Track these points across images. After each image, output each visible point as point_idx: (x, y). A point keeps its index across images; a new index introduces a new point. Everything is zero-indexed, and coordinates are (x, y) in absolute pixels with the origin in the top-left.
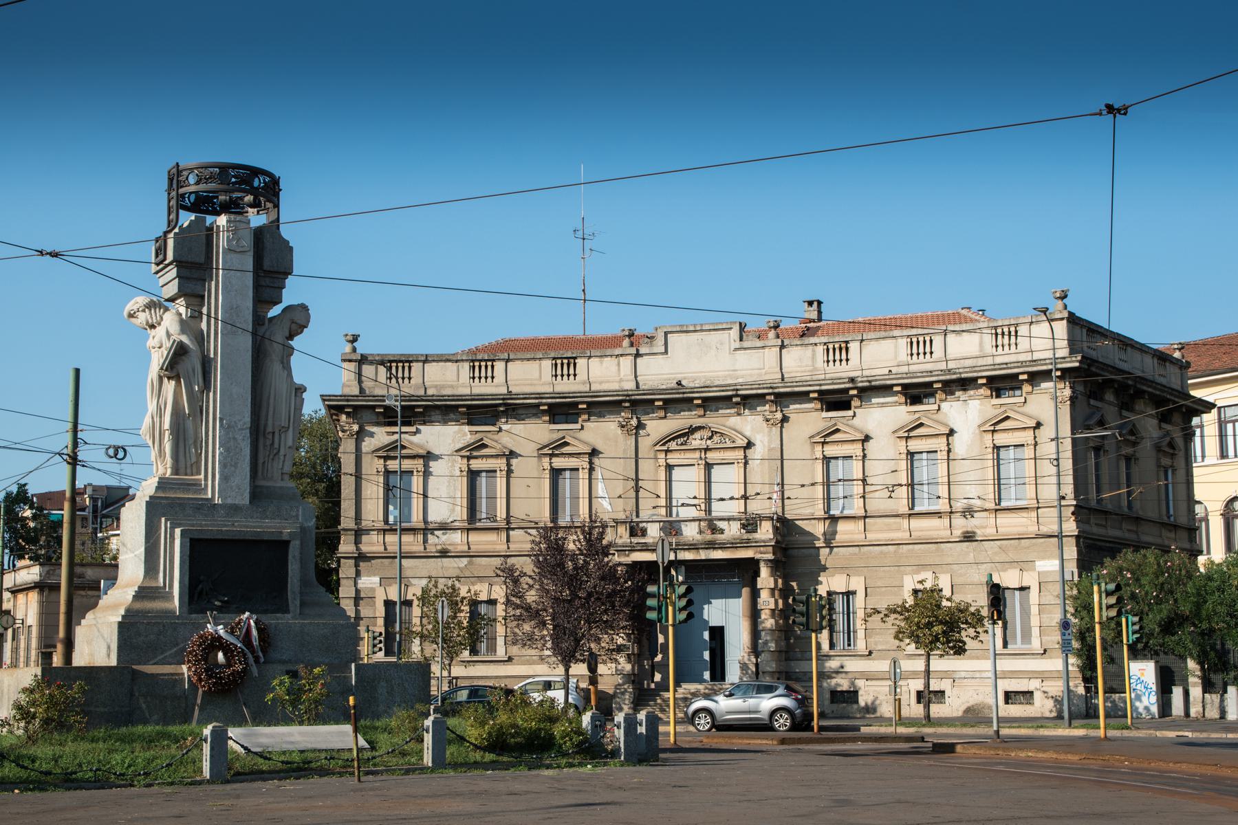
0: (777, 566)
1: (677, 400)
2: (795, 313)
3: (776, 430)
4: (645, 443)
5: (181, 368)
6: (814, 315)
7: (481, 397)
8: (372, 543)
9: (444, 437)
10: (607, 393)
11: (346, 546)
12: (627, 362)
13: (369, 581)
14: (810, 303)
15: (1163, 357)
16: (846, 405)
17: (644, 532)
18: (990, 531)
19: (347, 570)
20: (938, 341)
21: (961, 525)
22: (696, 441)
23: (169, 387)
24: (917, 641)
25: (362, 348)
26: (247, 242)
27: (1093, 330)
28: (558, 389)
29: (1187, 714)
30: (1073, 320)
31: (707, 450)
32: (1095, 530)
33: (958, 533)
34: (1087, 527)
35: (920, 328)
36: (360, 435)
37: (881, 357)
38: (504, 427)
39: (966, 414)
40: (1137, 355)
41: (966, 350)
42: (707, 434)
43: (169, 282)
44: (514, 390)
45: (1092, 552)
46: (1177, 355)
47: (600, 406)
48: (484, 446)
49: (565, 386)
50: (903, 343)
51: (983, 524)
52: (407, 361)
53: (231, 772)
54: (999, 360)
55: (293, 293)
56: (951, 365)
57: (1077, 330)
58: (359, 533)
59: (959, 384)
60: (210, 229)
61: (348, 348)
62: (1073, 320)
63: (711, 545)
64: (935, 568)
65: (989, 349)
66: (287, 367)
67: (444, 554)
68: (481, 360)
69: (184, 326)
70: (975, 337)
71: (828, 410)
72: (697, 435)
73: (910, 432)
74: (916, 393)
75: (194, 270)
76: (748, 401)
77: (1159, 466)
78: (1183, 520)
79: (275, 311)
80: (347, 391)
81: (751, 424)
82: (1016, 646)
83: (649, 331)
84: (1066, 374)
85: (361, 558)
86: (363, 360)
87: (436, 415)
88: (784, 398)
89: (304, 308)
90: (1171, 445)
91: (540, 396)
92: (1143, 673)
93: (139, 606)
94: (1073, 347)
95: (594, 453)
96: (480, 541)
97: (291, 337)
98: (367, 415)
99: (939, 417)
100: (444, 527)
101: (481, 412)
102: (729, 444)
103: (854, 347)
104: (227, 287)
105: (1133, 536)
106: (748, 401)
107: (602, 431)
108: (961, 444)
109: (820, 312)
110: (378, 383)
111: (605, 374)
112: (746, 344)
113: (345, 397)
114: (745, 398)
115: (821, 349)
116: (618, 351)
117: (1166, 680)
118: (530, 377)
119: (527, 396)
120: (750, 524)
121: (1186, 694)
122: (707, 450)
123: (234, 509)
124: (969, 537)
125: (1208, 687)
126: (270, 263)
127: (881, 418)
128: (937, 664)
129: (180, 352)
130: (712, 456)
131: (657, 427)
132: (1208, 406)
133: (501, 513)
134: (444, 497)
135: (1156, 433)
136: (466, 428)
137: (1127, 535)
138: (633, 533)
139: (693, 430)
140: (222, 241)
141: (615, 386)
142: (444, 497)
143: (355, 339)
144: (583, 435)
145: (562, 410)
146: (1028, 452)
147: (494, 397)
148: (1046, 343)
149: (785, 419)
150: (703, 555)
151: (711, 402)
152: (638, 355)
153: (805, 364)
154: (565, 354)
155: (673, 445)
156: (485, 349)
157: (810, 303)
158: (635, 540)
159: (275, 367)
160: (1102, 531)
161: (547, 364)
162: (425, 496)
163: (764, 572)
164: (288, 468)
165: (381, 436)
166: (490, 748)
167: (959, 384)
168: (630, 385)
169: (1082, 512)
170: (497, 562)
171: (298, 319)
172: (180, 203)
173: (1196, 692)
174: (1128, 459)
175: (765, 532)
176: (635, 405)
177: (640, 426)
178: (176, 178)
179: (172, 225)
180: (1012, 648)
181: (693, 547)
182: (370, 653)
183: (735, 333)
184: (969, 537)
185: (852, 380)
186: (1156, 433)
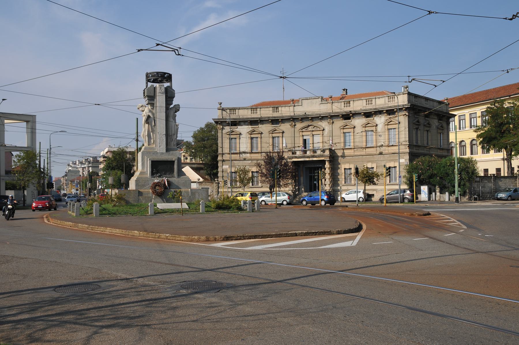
0: (330, 161)
1: (304, 118)
2: (339, 93)
3: (331, 125)
4: (296, 130)
5: (149, 121)
6: (345, 93)
7: (253, 118)
8: (226, 157)
9: (244, 129)
10: (286, 116)
11: (220, 158)
12: (292, 108)
13: (226, 167)
14: (344, 90)
15: (440, 103)
16: (349, 119)
17: (295, 153)
18: (387, 152)
19: (220, 164)
20: (374, 100)
21: (379, 150)
22: (310, 129)
23: (147, 125)
24: (362, 181)
25: (223, 106)
26: (163, 90)
27: (416, 96)
28: (274, 116)
29: (435, 200)
30: (409, 94)
31: (313, 131)
32: (415, 151)
33: (378, 152)
34: (412, 150)
35: (369, 97)
36: (223, 129)
37: (358, 106)
38: (260, 126)
39: (380, 120)
40: (432, 102)
41: (381, 103)
42: (312, 127)
43: (145, 101)
44: (263, 116)
45: (412, 156)
46: (446, 101)
47: (284, 120)
48: (255, 131)
49: (276, 115)
50: (365, 101)
51: (384, 150)
52: (234, 109)
53: (158, 212)
54: (389, 105)
55: (175, 102)
56: (377, 107)
57: (411, 97)
58: (223, 154)
59: (379, 112)
60: (155, 88)
61: (219, 106)
62: (409, 94)
63: (313, 157)
64: (372, 162)
65: (343, 107)
66: (175, 120)
67: (245, 159)
68: (254, 108)
69: (150, 111)
70: (383, 99)
71: (345, 120)
72: (310, 127)
73: (366, 125)
74: (368, 115)
75: (151, 98)
76: (322, 118)
77: (438, 133)
78: (446, 147)
79: (172, 106)
80: (219, 118)
81: (324, 124)
82: (393, 182)
83: (298, 99)
84: (407, 109)
85: (223, 161)
86: (223, 110)
87: (242, 123)
88: (332, 117)
89: (179, 105)
90: (442, 127)
91: (269, 117)
92: (424, 189)
93: (140, 176)
94: (409, 101)
95: (283, 132)
96: (254, 156)
97: (176, 112)
98: (224, 124)
99: (374, 121)
100: (244, 153)
101: (253, 122)
102: (318, 129)
103: (351, 102)
104: (161, 100)
105: (428, 152)
106: (322, 118)
107: (285, 127)
108: (380, 128)
109: (346, 92)
110: (227, 116)
111: (285, 111)
112: (323, 102)
113: (219, 119)
114: (323, 117)
115: (343, 103)
116: (289, 105)
117: (430, 193)
118: (267, 113)
119: (265, 118)
120: (324, 151)
121: (436, 194)
122: (313, 131)
123: (162, 153)
124: (381, 153)
125: (441, 193)
126: (169, 95)
127: (358, 122)
128: (368, 187)
129: (149, 117)
130: (314, 133)
131: (299, 125)
132: (454, 116)
133: (475, 124)
134: (244, 145)
135: (437, 124)
136: (250, 126)
137: (426, 152)
138: (293, 154)
139: (309, 126)
140: (158, 90)
141: (288, 114)
142: (244, 145)
143: (221, 104)
144: (280, 128)
145: (275, 121)
146: (397, 130)
147: (257, 118)
148: (403, 100)
149: (333, 123)
150: (311, 159)
151: (313, 119)
152: (294, 106)
153: (339, 108)
154: (275, 105)
155: (304, 130)
156: (255, 106)
157: (344, 90)
158: (293, 155)
159: (171, 119)
160: (417, 151)
161: (271, 109)
162: (222, 147)
163: (327, 163)
164: (175, 143)
165: (227, 129)
166: (216, 208)
167: (379, 112)
168: (292, 114)
169: (410, 146)
170: (255, 161)
171: (177, 108)
172: (148, 81)
173: (438, 194)
174: (427, 131)
175: (327, 153)
176: (293, 119)
177: (295, 125)
178: (147, 75)
179: (147, 86)
180: (391, 183)
181: (308, 157)
182: (482, 174)
183: (320, 99)
184: (381, 153)
185: (350, 111)
186: (437, 124)
